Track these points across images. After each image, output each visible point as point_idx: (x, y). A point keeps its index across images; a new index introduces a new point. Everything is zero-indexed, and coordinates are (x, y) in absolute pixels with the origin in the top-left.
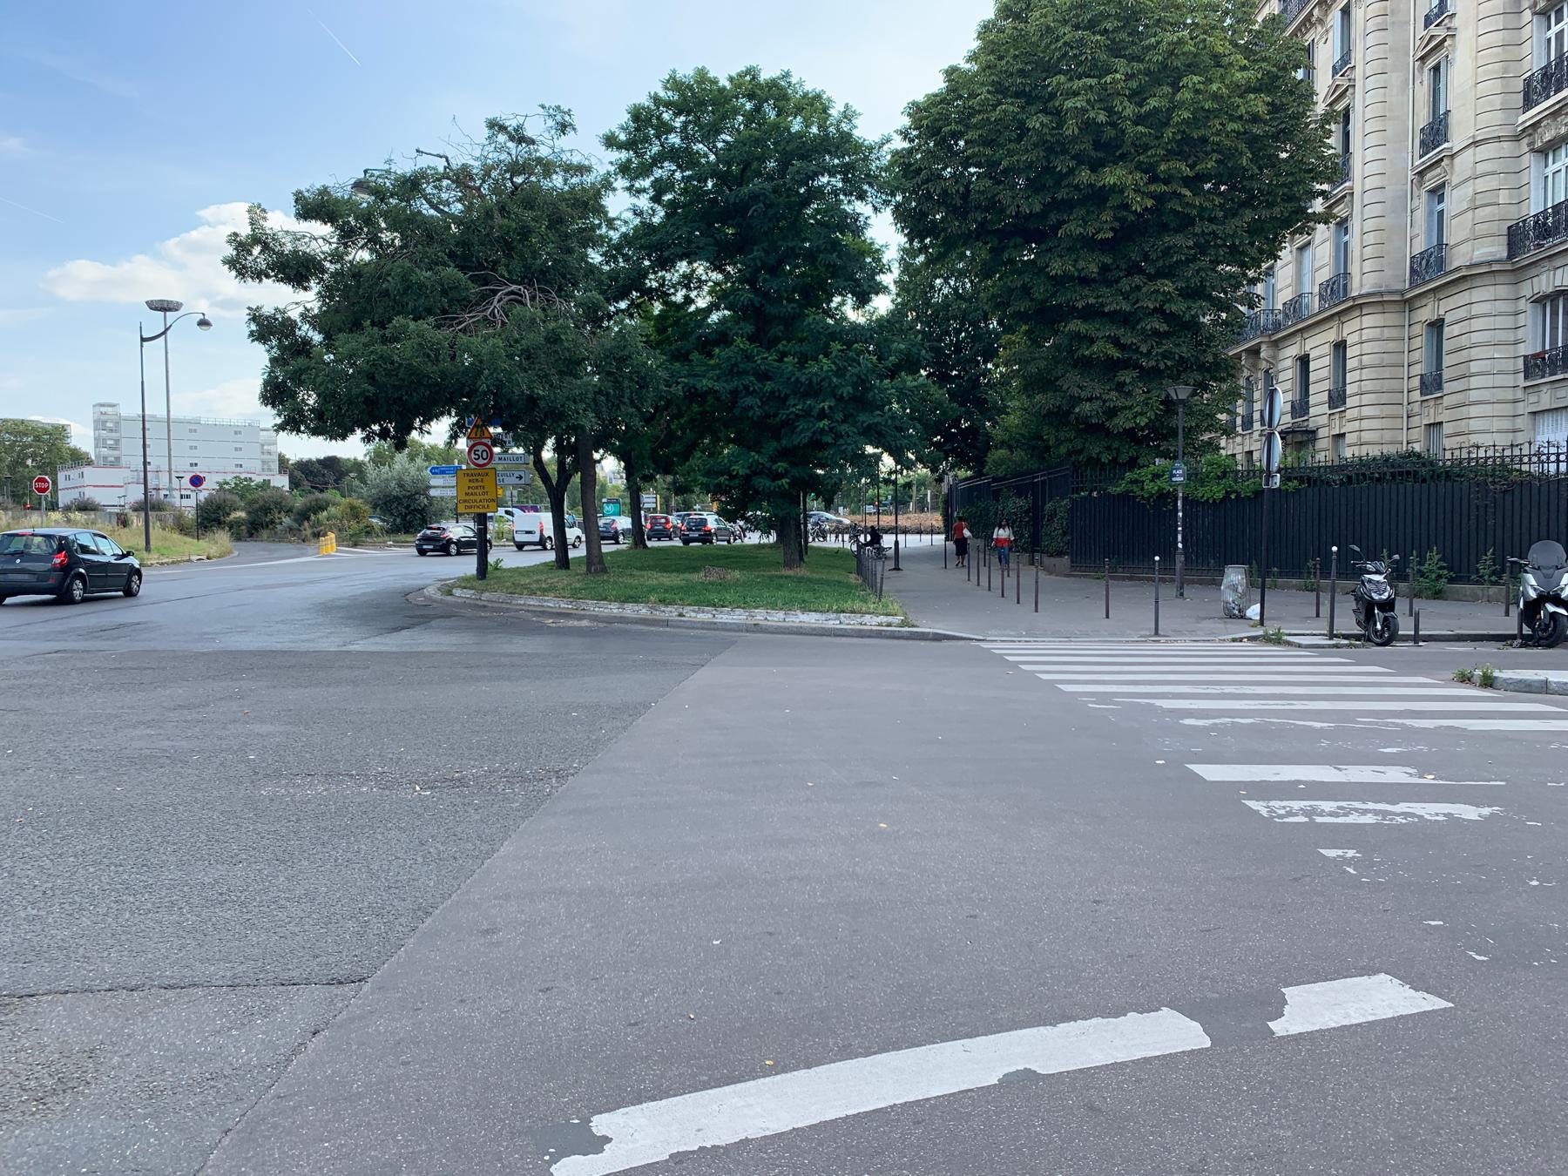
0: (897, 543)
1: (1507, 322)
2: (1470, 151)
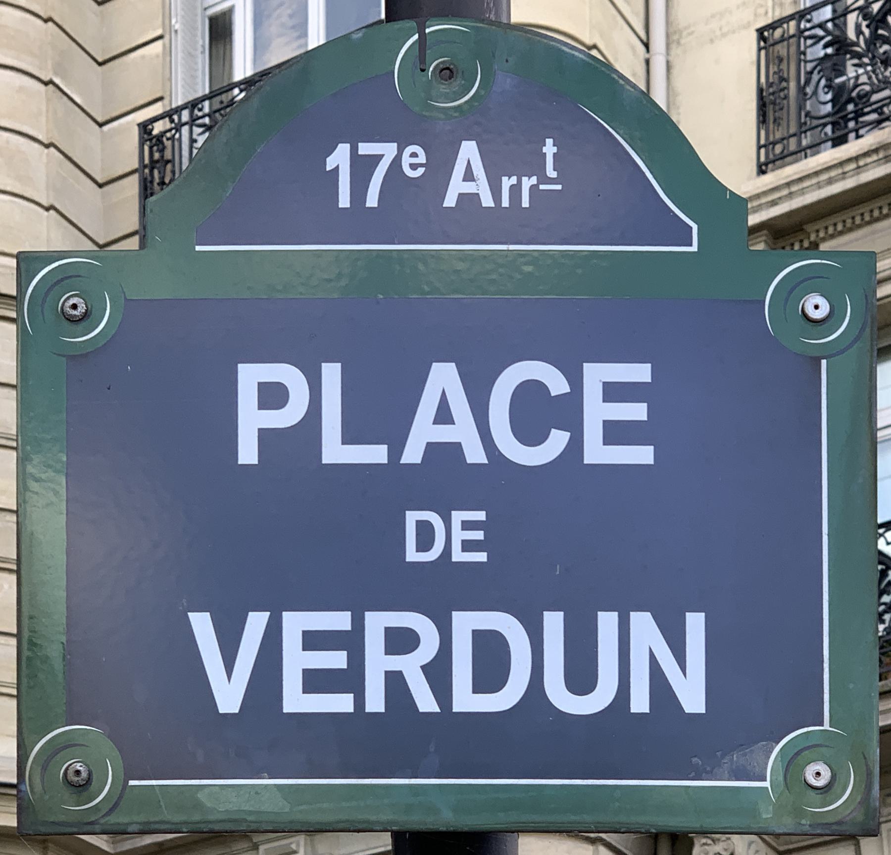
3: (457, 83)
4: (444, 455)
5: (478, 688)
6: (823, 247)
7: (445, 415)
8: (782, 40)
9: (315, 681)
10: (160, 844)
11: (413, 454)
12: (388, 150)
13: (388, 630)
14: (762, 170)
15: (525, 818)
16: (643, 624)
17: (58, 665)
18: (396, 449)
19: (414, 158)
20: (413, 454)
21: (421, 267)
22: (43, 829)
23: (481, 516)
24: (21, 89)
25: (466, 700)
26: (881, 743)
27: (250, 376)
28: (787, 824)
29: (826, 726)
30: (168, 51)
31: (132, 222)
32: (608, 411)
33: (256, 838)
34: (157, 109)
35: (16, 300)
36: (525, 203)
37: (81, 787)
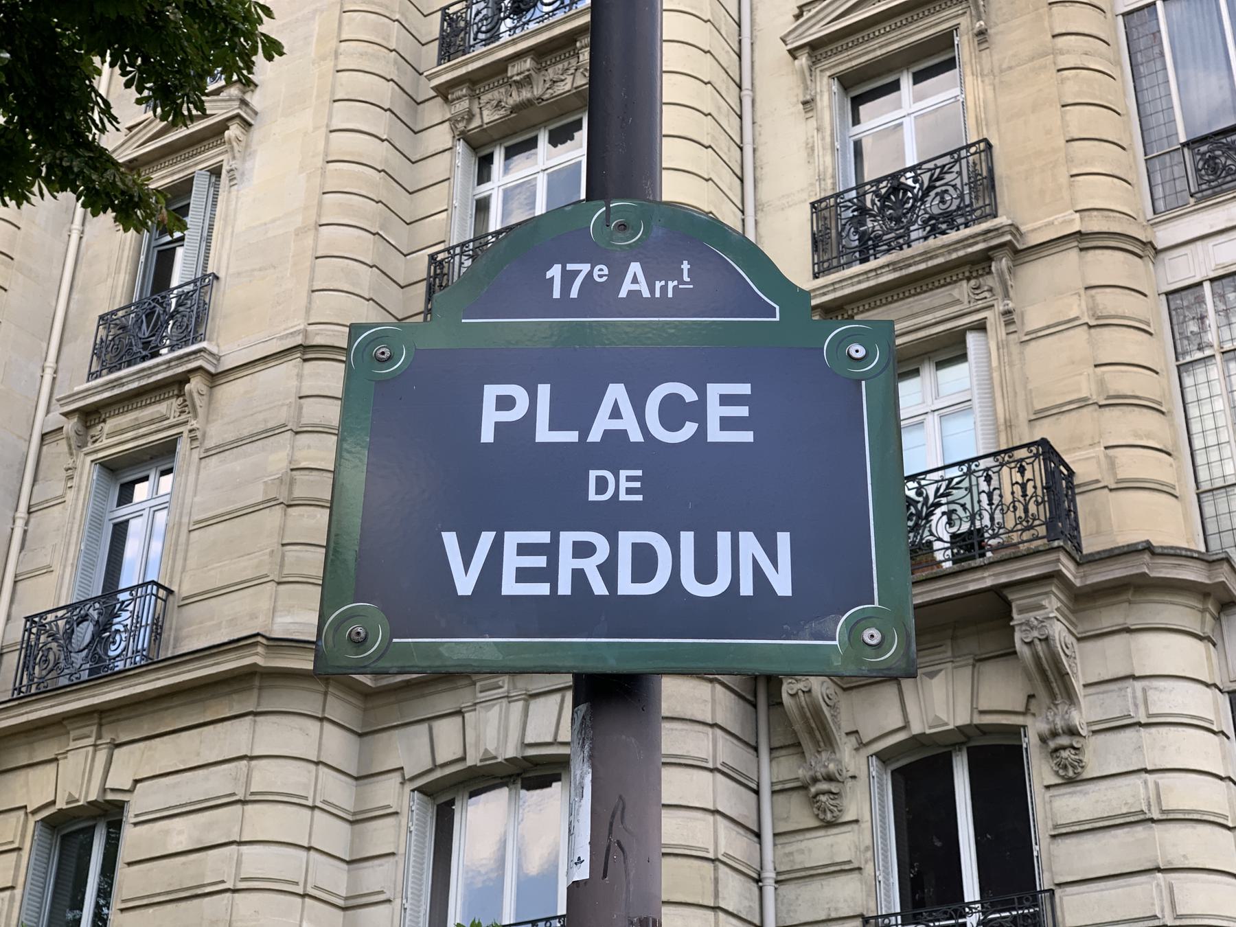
0: (324, 710)
1: (333, 835)
2: (290, 367)
3: (628, 232)
4: (615, 438)
5: (635, 579)
6: (857, 318)
7: (616, 412)
8: (826, 208)
9: (523, 575)
10: (408, 681)
11: (595, 436)
12: (585, 268)
13: (575, 543)
14: (816, 276)
15: (667, 665)
16: (748, 540)
17: (352, 565)
18: (584, 434)
19: (601, 272)
20: (595, 436)
21: (603, 330)
22: (330, 671)
23: (639, 473)
24: (359, 237)
25: (627, 586)
26: (916, 617)
27: (491, 392)
28: (851, 669)
29: (876, 604)
30: (450, 218)
31: (420, 306)
32: (722, 413)
33: (475, 678)
34: (441, 247)
35: (347, 351)
36: (670, 295)
37: (360, 643)
